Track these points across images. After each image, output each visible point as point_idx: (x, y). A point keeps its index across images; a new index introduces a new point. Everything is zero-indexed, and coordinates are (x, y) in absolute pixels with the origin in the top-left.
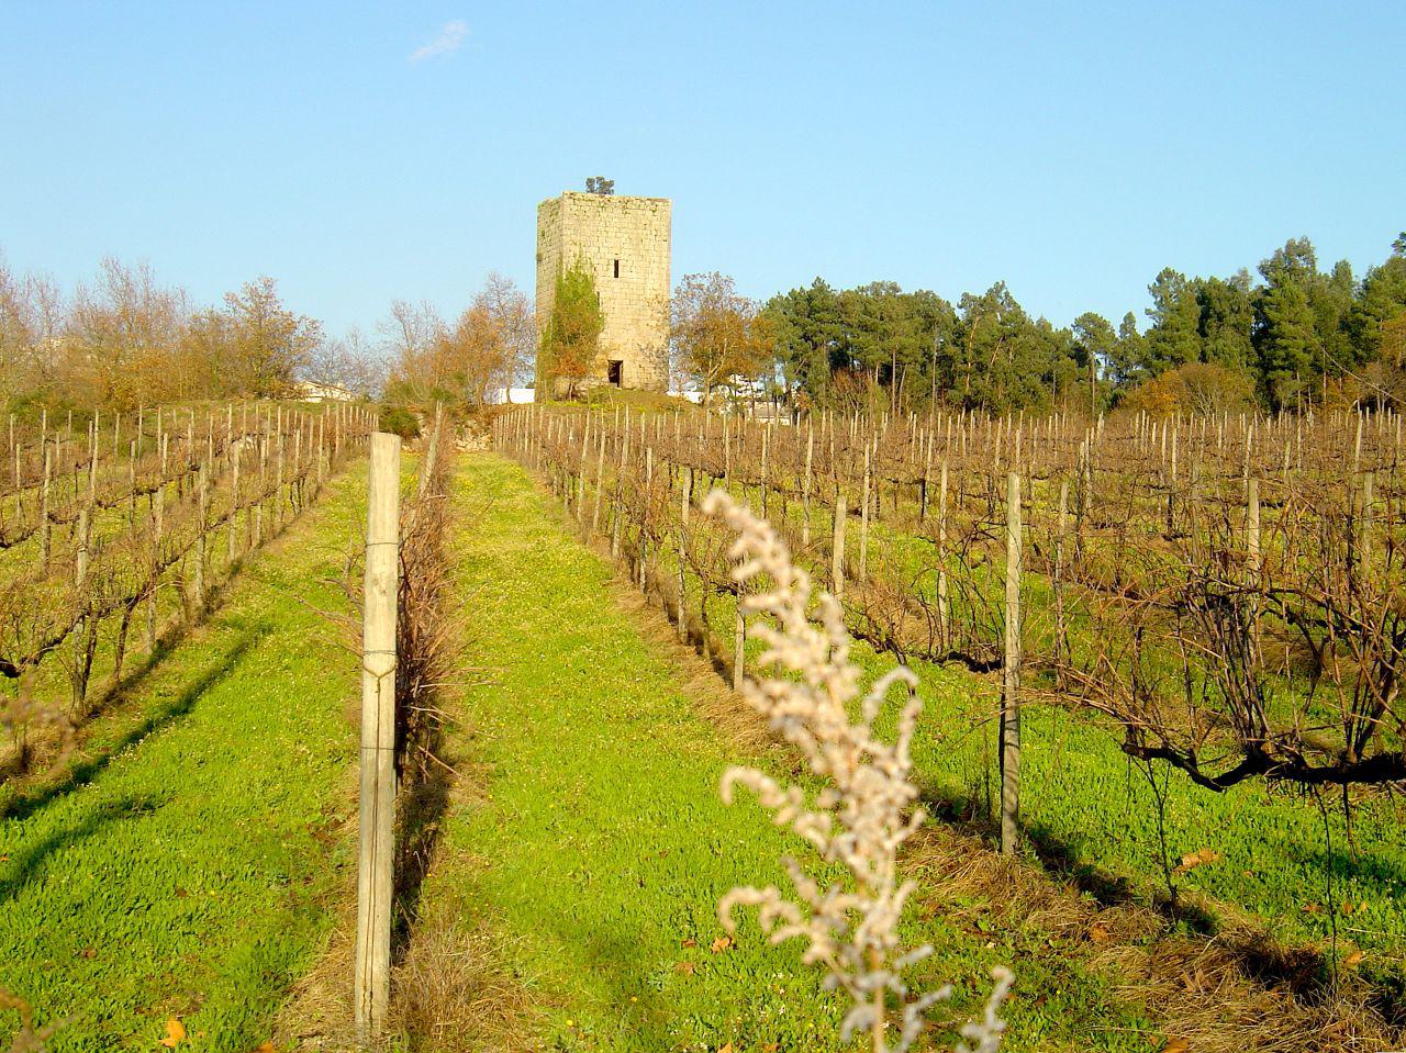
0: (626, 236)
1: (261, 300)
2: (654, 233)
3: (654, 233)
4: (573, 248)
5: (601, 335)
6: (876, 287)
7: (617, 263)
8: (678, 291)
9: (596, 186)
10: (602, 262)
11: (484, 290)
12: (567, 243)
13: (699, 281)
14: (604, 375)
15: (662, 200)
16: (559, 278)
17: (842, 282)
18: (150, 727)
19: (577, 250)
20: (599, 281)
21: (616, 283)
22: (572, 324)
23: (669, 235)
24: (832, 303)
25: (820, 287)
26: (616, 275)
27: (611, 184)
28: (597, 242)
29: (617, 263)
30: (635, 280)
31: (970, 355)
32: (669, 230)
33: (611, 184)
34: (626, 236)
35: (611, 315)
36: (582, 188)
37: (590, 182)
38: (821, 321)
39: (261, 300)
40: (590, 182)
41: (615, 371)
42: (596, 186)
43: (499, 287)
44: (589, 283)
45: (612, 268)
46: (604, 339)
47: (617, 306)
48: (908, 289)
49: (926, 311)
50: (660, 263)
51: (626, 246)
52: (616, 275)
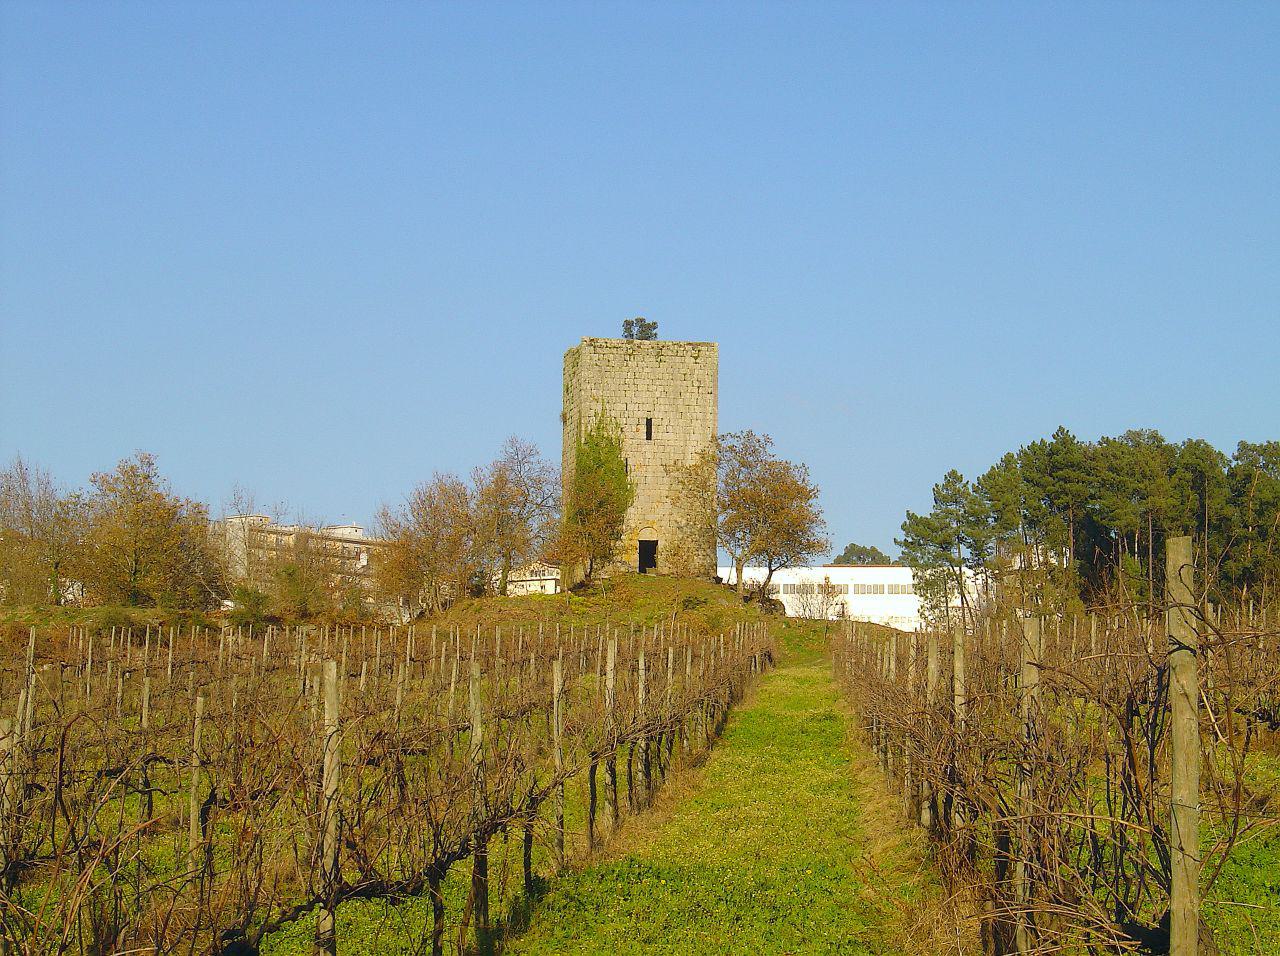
0: (661, 389)
1: (136, 481)
2: (696, 384)
3: (696, 384)
4: (594, 405)
5: (630, 510)
6: (1134, 437)
7: (649, 422)
8: (702, 455)
9: (635, 330)
10: (629, 421)
11: (501, 458)
12: (586, 400)
13: (730, 442)
14: (634, 558)
15: (704, 344)
16: (578, 440)
17: (1088, 434)
18: (617, 816)
19: (599, 408)
20: (627, 444)
21: (648, 447)
22: (597, 491)
23: (716, 387)
24: (1077, 457)
25: (1064, 439)
26: (649, 437)
27: (654, 326)
28: (630, 396)
29: (649, 422)
30: (672, 443)
31: (1251, 516)
32: (715, 381)
33: (654, 326)
34: (661, 389)
35: (641, 486)
36: (616, 335)
37: (628, 324)
38: (1066, 480)
39: (136, 481)
40: (628, 324)
41: (648, 551)
42: (635, 330)
43: (520, 455)
44: (615, 447)
45: (643, 429)
46: (632, 516)
47: (649, 475)
48: (1174, 437)
49: (1194, 467)
50: (705, 420)
51: (661, 401)
52: (649, 437)
